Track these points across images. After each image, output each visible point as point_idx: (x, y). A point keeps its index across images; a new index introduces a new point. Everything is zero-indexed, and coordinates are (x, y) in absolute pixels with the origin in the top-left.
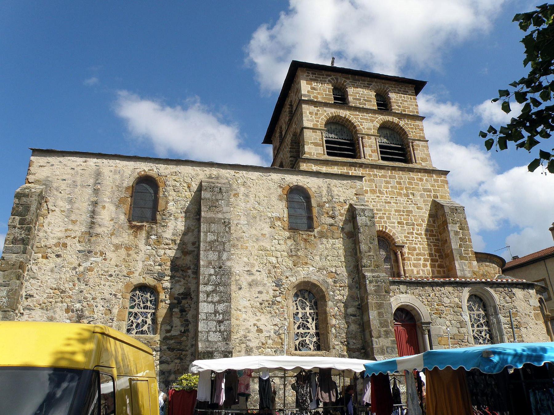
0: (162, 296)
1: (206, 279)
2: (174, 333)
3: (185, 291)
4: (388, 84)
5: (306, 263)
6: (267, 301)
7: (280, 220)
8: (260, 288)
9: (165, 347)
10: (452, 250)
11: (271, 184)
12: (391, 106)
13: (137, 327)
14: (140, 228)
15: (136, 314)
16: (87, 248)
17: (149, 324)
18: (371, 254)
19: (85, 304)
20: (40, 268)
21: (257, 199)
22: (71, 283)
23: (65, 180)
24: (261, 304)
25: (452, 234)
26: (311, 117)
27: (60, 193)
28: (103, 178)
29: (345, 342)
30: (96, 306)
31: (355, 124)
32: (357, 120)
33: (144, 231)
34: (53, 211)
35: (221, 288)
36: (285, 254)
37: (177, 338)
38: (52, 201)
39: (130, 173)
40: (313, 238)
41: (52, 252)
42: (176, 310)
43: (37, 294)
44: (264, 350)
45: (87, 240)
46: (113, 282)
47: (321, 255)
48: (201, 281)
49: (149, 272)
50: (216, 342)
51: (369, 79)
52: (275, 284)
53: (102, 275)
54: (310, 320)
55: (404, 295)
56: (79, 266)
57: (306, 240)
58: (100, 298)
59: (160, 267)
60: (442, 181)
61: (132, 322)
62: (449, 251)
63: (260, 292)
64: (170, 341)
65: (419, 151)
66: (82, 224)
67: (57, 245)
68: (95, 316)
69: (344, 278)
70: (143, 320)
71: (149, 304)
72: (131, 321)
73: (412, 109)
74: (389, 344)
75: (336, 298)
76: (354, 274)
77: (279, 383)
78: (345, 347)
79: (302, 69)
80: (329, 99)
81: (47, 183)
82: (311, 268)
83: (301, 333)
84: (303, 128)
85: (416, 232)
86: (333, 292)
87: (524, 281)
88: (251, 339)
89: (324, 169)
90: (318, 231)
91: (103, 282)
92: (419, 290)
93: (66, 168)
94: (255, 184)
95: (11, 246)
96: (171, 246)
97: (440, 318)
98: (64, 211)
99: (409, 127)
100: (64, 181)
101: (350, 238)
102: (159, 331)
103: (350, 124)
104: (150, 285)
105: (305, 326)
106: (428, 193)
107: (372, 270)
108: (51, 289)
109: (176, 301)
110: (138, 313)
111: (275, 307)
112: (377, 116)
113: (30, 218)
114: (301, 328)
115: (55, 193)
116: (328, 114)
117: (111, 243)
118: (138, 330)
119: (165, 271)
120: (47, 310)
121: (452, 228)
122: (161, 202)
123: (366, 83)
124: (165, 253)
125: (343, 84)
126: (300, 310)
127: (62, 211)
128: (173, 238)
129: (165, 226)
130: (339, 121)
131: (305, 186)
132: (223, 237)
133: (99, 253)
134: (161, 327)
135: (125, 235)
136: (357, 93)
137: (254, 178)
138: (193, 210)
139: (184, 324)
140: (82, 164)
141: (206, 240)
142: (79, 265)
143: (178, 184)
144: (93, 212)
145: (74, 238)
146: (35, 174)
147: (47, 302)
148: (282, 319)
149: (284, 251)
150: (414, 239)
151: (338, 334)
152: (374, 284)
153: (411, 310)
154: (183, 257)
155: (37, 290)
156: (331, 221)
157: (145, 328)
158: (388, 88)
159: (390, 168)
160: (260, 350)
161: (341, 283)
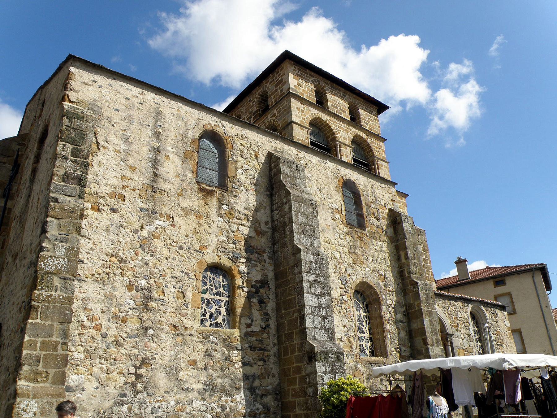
0: (239, 281)
1: (307, 266)
2: (255, 328)
3: (262, 279)
9: (247, 345)
12: (360, 122)
14: (211, 193)
15: (208, 301)
17: (224, 315)
19: (151, 281)
21: (318, 185)
23: (118, 110)
26: (298, 113)
27: (113, 126)
28: (164, 120)
29: (398, 348)
30: (167, 286)
31: (334, 131)
33: (215, 198)
34: (104, 148)
37: (258, 335)
38: (103, 134)
39: (194, 122)
41: (105, 204)
42: (254, 300)
43: (88, 259)
50: (323, 341)
51: (344, 90)
52: (340, 281)
53: (171, 245)
54: (364, 323)
56: (141, 229)
59: (234, 246)
64: (251, 338)
65: (382, 171)
66: (143, 174)
67: (112, 195)
68: (166, 298)
69: (391, 282)
71: (222, 290)
72: (203, 309)
75: (388, 302)
76: (398, 280)
78: (398, 354)
79: (290, 61)
81: (93, 106)
82: (367, 269)
84: (292, 122)
86: (386, 296)
87: (500, 303)
91: (172, 256)
93: (119, 95)
95: (62, 183)
98: (119, 152)
102: (237, 324)
104: (225, 265)
105: (361, 330)
108: (106, 254)
109: (254, 290)
110: (210, 300)
112: (350, 127)
113: (87, 151)
115: (107, 124)
116: (312, 114)
118: (212, 322)
120: (104, 284)
122: (231, 167)
124: (238, 230)
125: (323, 88)
128: (246, 212)
129: (237, 196)
130: (318, 124)
132: (312, 221)
133: (165, 216)
134: (240, 320)
135: (194, 198)
136: (335, 101)
138: (263, 184)
139: (264, 318)
140: (139, 96)
142: (142, 228)
144: (156, 161)
145: (134, 190)
146: (77, 92)
148: (350, 320)
149: (345, 247)
151: (393, 340)
154: (256, 237)
155: (88, 253)
157: (220, 320)
158: (358, 104)
161: (390, 288)
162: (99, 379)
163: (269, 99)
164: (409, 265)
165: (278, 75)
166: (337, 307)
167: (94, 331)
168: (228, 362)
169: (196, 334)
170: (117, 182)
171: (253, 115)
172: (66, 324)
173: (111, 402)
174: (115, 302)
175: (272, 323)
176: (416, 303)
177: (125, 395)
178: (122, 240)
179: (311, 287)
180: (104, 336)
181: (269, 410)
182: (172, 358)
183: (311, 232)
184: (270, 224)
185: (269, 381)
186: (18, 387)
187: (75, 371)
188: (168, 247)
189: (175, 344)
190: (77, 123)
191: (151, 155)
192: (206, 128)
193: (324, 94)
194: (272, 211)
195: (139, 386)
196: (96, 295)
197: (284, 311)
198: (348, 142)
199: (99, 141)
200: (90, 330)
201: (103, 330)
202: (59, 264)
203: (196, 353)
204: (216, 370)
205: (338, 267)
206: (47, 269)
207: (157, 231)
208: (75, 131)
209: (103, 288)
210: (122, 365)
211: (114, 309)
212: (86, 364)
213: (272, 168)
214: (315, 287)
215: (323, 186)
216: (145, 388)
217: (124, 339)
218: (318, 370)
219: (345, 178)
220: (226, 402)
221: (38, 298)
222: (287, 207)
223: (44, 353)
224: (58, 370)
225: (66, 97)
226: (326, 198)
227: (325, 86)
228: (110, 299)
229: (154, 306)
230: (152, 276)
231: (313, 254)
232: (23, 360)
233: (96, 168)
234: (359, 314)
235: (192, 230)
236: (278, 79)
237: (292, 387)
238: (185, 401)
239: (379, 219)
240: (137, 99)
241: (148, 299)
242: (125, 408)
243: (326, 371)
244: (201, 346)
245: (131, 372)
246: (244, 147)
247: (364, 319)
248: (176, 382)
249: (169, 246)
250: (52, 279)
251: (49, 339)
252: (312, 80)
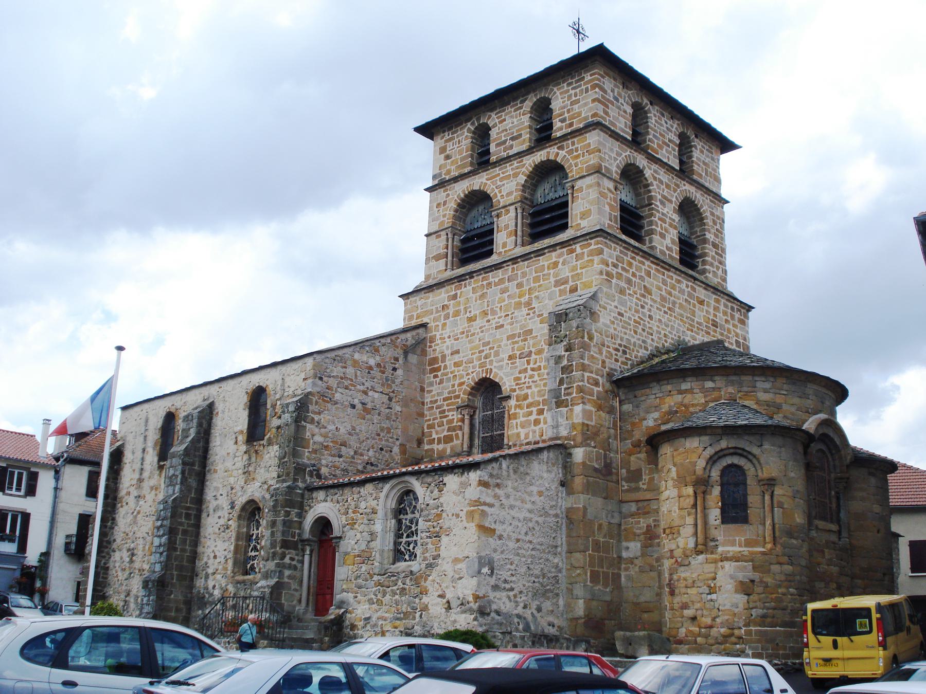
51: (523, 90)
55: (324, 504)
92: (338, 495)
150: (527, 380)
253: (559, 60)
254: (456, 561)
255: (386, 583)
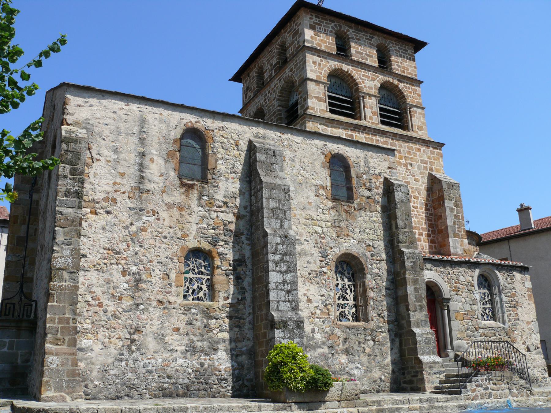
1: (274, 247)
4: (389, 39)
5: (348, 235)
6: (315, 271)
7: (324, 189)
8: (309, 258)
10: (447, 227)
11: (314, 150)
12: (391, 65)
13: (193, 293)
14: (192, 187)
15: (191, 280)
16: (138, 205)
17: (205, 291)
18: (406, 230)
19: (141, 267)
20: (90, 225)
21: (302, 164)
22: (124, 244)
23: (107, 125)
24: (310, 274)
25: (448, 210)
26: (314, 67)
27: (104, 139)
30: (154, 270)
32: (359, 77)
34: (97, 160)
35: (288, 258)
36: (329, 224)
38: (96, 148)
39: (176, 123)
40: (353, 210)
43: (90, 254)
44: (313, 319)
45: (137, 197)
46: (169, 245)
47: (360, 227)
48: (269, 250)
49: (204, 236)
50: (286, 312)
51: (371, 31)
53: (156, 236)
54: (348, 291)
55: (429, 272)
57: (347, 212)
58: (156, 261)
59: (213, 231)
60: (438, 154)
61: (188, 288)
62: (443, 228)
63: (308, 262)
65: (416, 118)
66: (131, 178)
67: (106, 199)
68: (153, 280)
70: (198, 286)
71: (203, 269)
72: (186, 286)
73: (411, 71)
74: (423, 318)
75: (374, 271)
77: (328, 352)
80: (332, 49)
81: (87, 126)
82: (352, 240)
83: (341, 304)
85: (413, 205)
86: (371, 265)
87: (522, 264)
88: (302, 309)
89: (330, 131)
90: (357, 203)
91: (158, 244)
93: (107, 111)
94: (299, 147)
96: (223, 209)
97: (457, 295)
98: (109, 161)
99: (407, 91)
100: (106, 126)
101: (385, 212)
103: (351, 80)
104: (205, 249)
105: (344, 298)
106: (425, 165)
107: (407, 246)
108: (104, 249)
111: (322, 277)
114: (341, 300)
117: (163, 201)
118: (195, 297)
119: (219, 236)
120: (103, 272)
121: (449, 204)
122: (211, 159)
123: (368, 35)
124: (218, 217)
125: (345, 33)
126: (340, 282)
127: (108, 161)
128: (225, 200)
130: (339, 75)
131: (345, 155)
132: (284, 205)
133: (151, 212)
135: (176, 194)
137: (299, 141)
139: (240, 292)
141: (269, 206)
142: (132, 224)
143: (226, 141)
144: (141, 165)
145: (124, 193)
146: (73, 114)
147: (101, 263)
151: (376, 307)
152: (411, 260)
153: (433, 286)
155: (90, 249)
156: (368, 193)
157: (201, 294)
158: (389, 44)
159: (392, 135)
160: (310, 320)
162: (103, 343)
163: (287, 51)
164: (398, 235)
165: (295, 24)
166: (315, 279)
167: (98, 308)
168: (206, 329)
169: (179, 307)
170: (109, 188)
171: (274, 68)
172: (74, 305)
173: (113, 359)
174: (112, 285)
175: (249, 296)
176: (402, 271)
177: (123, 354)
178: (116, 236)
179: (276, 266)
180: (105, 311)
181: (243, 367)
182: (160, 326)
183: (282, 215)
184: (249, 208)
185: (244, 344)
186: (46, 348)
187: (86, 337)
188: (154, 238)
189: (161, 316)
190: (72, 146)
191: (138, 160)
192: (187, 127)
193: (347, 40)
194: (251, 196)
195: (134, 348)
196: (97, 281)
197: (257, 286)
198: (374, 92)
199: (93, 155)
200: (94, 307)
201: (104, 307)
202: (66, 261)
203: (179, 322)
204: (196, 335)
205: (319, 241)
206: (58, 266)
207: (145, 225)
208: (71, 154)
209: (103, 275)
210: (120, 333)
211: (112, 291)
212: (93, 332)
213: (252, 155)
214: (280, 265)
215: (307, 164)
216: (138, 349)
217: (120, 313)
218: (276, 336)
219: (333, 153)
220: (205, 360)
221: (54, 287)
222: (260, 193)
223: (61, 325)
224: (71, 337)
225: (64, 122)
226: (310, 177)
227: (348, 31)
228: (108, 283)
229: (144, 287)
230: (141, 263)
231: (281, 236)
232: (47, 330)
233: (92, 179)
234: (343, 282)
235: (175, 221)
236: (295, 29)
237: (261, 349)
238: (170, 359)
239: (370, 190)
240: (123, 111)
241: (138, 281)
242: (123, 363)
243: (284, 336)
244: (183, 316)
245: (127, 337)
246: (225, 138)
247: (349, 287)
248: (163, 345)
249: (155, 237)
250: (62, 273)
251: (63, 316)
252: (332, 27)
253: (407, 34)
254: (528, 323)
255: (490, 335)
